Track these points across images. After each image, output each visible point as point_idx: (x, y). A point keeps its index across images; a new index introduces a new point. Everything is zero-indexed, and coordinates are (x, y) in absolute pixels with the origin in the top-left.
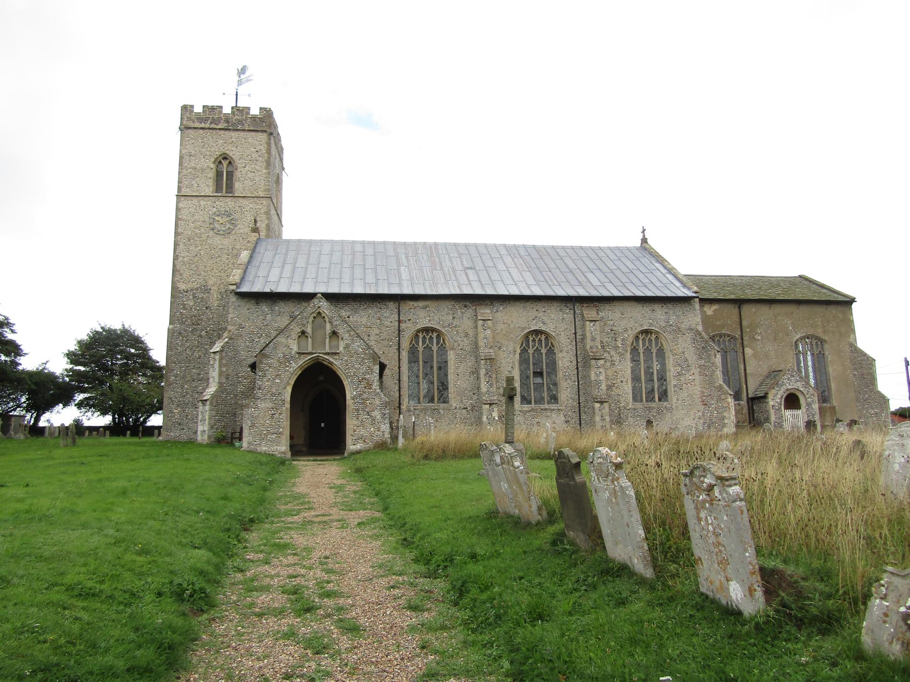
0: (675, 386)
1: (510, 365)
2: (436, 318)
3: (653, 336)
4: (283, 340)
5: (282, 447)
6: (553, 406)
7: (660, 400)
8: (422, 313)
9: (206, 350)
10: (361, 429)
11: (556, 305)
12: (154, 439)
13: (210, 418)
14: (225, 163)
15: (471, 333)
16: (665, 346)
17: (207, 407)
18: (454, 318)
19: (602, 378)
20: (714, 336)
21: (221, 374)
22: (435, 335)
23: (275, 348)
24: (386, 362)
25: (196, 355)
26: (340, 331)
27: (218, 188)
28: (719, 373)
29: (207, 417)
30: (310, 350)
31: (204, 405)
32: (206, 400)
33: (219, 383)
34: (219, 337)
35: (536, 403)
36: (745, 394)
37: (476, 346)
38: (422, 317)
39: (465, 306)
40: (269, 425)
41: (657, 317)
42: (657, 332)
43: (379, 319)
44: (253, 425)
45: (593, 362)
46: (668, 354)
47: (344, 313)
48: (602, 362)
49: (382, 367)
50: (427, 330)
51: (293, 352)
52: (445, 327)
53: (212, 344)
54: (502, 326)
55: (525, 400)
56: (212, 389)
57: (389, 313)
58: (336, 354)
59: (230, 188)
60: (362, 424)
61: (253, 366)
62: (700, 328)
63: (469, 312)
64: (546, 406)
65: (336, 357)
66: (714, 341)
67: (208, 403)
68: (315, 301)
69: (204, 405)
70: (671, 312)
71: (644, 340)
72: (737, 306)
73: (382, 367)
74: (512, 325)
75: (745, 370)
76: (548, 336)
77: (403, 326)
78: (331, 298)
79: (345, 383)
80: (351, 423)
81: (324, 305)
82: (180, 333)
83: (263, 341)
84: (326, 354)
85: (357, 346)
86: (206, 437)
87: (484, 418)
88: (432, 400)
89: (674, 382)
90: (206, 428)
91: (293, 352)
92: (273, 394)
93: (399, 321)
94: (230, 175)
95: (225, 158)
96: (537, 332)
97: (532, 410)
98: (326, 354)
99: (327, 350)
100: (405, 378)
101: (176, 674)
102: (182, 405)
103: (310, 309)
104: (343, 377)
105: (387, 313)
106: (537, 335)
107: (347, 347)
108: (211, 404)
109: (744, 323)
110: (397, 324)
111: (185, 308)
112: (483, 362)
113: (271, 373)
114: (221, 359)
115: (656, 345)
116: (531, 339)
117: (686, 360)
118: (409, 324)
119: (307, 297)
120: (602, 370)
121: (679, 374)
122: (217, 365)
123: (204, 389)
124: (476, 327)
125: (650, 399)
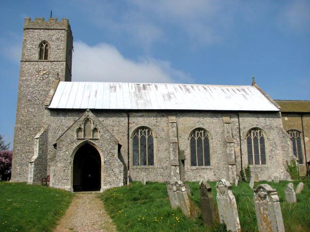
0: (270, 156)
1: (185, 145)
2: (148, 121)
3: (258, 131)
4: (71, 133)
5: (68, 187)
6: (208, 167)
7: (262, 163)
8: (140, 119)
9: (33, 137)
10: (111, 178)
11: (155, 114)
12: (7, 182)
13: (34, 171)
14: (44, 46)
15: (165, 129)
16: (264, 136)
17: (33, 166)
18: (157, 122)
19: (233, 152)
20: (289, 131)
21: (39, 150)
22: (203, 132)
23: (66, 136)
24: (121, 144)
25: (28, 140)
26: (98, 127)
27: (40, 58)
28: (291, 150)
29: (33, 171)
30: (83, 138)
31: (31, 165)
32: (32, 162)
33: (39, 153)
34: (39, 130)
35: (199, 165)
36: (305, 160)
37: (168, 136)
38: (139, 121)
39: (163, 116)
40: (61, 177)
41: (260, 122)
42: (260, 129)
43: (119, 122)
44: (55, 175)
45: (228, 144)
46: (266, 140)
47: (101, 119)
48: (232, 144)
49: (120, 146)
50: (143, 128)
51: (75, 139)
52: (152, 126)
53: (36, 134)
54: (182, 126)
55: (193, 163)
56: (35, 157)
57: (124, 120)
58: (96, 139)
59: (46, 57)
60: (109, 176)
61: (55, 145)
62: (282, 127)
63: (165, 119)
64: (204, 167)
65: (96, 141)
66: (289, 133)
67: (33, 163)
68: (86, 113)
69: (31, 165)
70: (267, 119)
71: (254, 133)
72: (300, 118)
73: (120, 146)
74: (186, 126)
75: (305, 148)
76: (205, 131)
77: (130, 125)
78: (94, 111)
79: (101, 154)
80: (103, 175)
81: (91, 114)
82: (21, 129)
83: (60, 133)
84: (91, 139)
85: (107, 136)
86: (32, 181)
87: (172, 173)
88: (145, 164)
89: (269, 154)
90: (32, 176)
91: (75, 139)
92: (65, 160)
93: (129, 123)
94: (46, 51)
95: (44, 43)
96: (199, 129)
97: (197, 169)
98: (91, 139)
99: (91, 137)
100: (131, 152)
101: (302, 204)
102: (21, 165)
103: (83, 117)
104: (100, 151)
105: (122, 119)
106: (199, 131)
107: (102, 136)
108: (35, 164)
109: (304, 125)
110: (127, 124)
111: (23, 116)
112: (171, 144)
113: (64, 149)
114: (39, 142)
115: (260, 136)
116: (196, 132)
117: (275, 143)
118: (134, 125)
119: (81, 111)
120: (232, 148)
121: (272, 150)
122: (38, 145)
123: (32, 157)
124: (168, 126)
125: (257, 163)
